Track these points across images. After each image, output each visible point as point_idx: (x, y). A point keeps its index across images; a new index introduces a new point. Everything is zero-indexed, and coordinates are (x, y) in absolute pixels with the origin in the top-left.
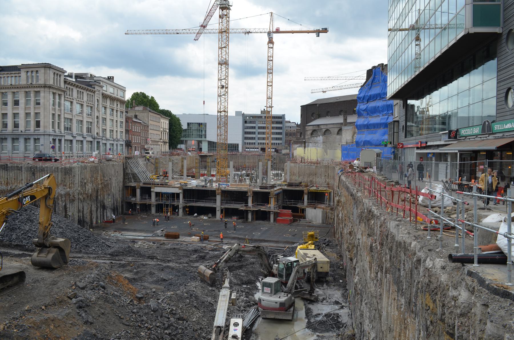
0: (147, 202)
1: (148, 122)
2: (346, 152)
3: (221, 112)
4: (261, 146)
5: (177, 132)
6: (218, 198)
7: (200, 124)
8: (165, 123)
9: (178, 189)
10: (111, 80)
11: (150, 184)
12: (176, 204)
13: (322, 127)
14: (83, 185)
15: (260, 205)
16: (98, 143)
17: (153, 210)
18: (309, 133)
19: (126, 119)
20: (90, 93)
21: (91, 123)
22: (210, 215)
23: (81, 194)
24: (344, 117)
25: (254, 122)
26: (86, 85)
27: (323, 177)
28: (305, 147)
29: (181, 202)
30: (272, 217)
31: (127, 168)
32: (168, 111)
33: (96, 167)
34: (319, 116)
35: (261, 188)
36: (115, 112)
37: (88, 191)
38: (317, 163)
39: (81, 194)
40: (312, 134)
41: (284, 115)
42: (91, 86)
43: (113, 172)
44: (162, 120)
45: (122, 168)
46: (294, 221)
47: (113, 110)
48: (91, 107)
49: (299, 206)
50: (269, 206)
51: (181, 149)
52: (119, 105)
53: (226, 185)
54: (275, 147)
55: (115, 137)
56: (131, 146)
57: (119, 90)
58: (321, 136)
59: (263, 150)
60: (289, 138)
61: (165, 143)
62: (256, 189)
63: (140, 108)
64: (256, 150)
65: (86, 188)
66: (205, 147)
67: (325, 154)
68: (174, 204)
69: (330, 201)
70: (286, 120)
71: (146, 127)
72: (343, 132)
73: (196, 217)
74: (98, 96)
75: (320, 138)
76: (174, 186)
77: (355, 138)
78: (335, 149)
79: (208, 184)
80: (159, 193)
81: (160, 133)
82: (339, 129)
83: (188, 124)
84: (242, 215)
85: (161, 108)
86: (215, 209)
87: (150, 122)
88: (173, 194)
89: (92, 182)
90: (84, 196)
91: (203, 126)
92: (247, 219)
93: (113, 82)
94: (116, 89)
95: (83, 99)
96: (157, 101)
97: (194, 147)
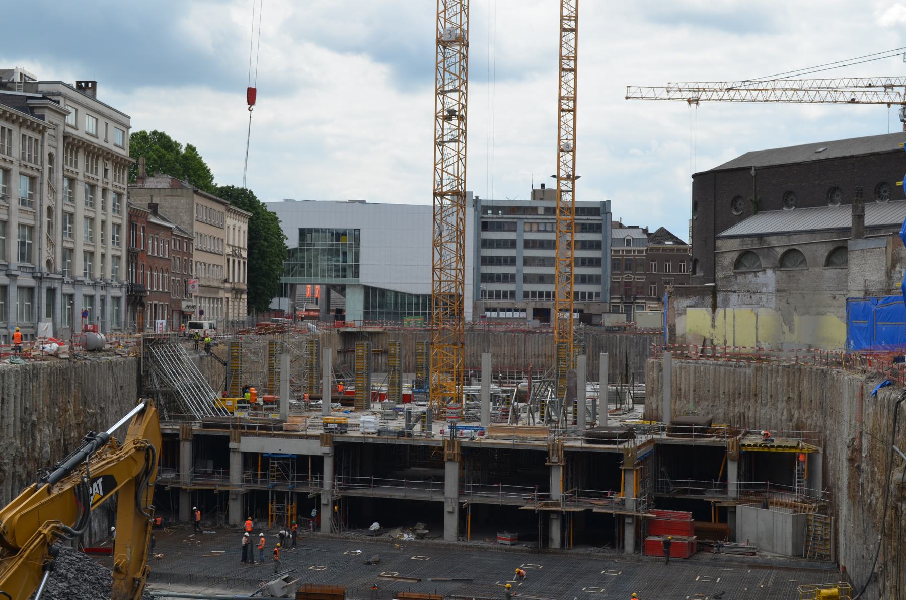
0: (216, 484)
1: (192, 225)
2: (863, 323)
3: (442, 195)
4: (532, 304)
5: (273, 256)
6: (452, 472)
7: (337, 235)
8: (236, 231)
9: (317, 443)
10: (88, 92)
11: (227, 427)
12: (310, 490)
13: (774, 241)
14: (28, 429)
15: (588, 495)
16: (51, 292)
17: (235, 510)
18: (728, 260)
19: (130, 216)
20: (29, 133)
21: (31, 228)
22: (421, 529)
23: (22, 460)
24: (855, 209)
25: (512, 227)
26: (16, 108)
27: (781, 405)
28: (714, 307)
29: (328, 485)
30: (629, 535)
31: (147, 373)
32: (228, 187)
33: (63, 372)
34: (759, 208)
35: (591, 438)
36: (99, 193)
37: (41, 449)
38: (759, 357)
39: (22, 460)
40: (738, 264)
41: (606, 205)
42: (31, 110)
43: (109, 388)
44: (230, 221)
45: (135, 375)
46: (701, 547)
47: (93, 187)
48: (32, 179)
49: (711, 496)
50: (617, 498)
51: (280, 313)
52: (110, 173)
53: (475, 429)
54: (579, 305)
55: (98, 275)
56: (143, 305)
57: (111, 125)
58: (769, 272)
59: (542, 314)
60: (628, 277)
61: (237, 292)
62: (577, 444)
63: (161, 182)
64: (517, 315)
65: (34, 440)
66: (354, 307)
67: (786, 328)
68: (303, 490)
69: (811, 482)
70: (615, 218)
71: (184, 242)
72: (854, 261)
73: (377, 533)
74: (52, 145)
75: (769, 278)
76: (306, 430)
77: (896, 276)
78: (819, 314)
79: (418, 428)
80: (255, 455)
81: (222, 261)
82: (831, 247)
83: (302, 232)
84: (529, 528)
85: (220, 181)
86: (438, 508)
87: (198, 227)
88: (301, 460)
89: (52, 419)
90: (30, 466)
91: (349, 241)
92: (547, 539)
93: (93, 97)
94: (102, 121)
95: (9, 154)
96: (204, 160)
97: (312, 306)
